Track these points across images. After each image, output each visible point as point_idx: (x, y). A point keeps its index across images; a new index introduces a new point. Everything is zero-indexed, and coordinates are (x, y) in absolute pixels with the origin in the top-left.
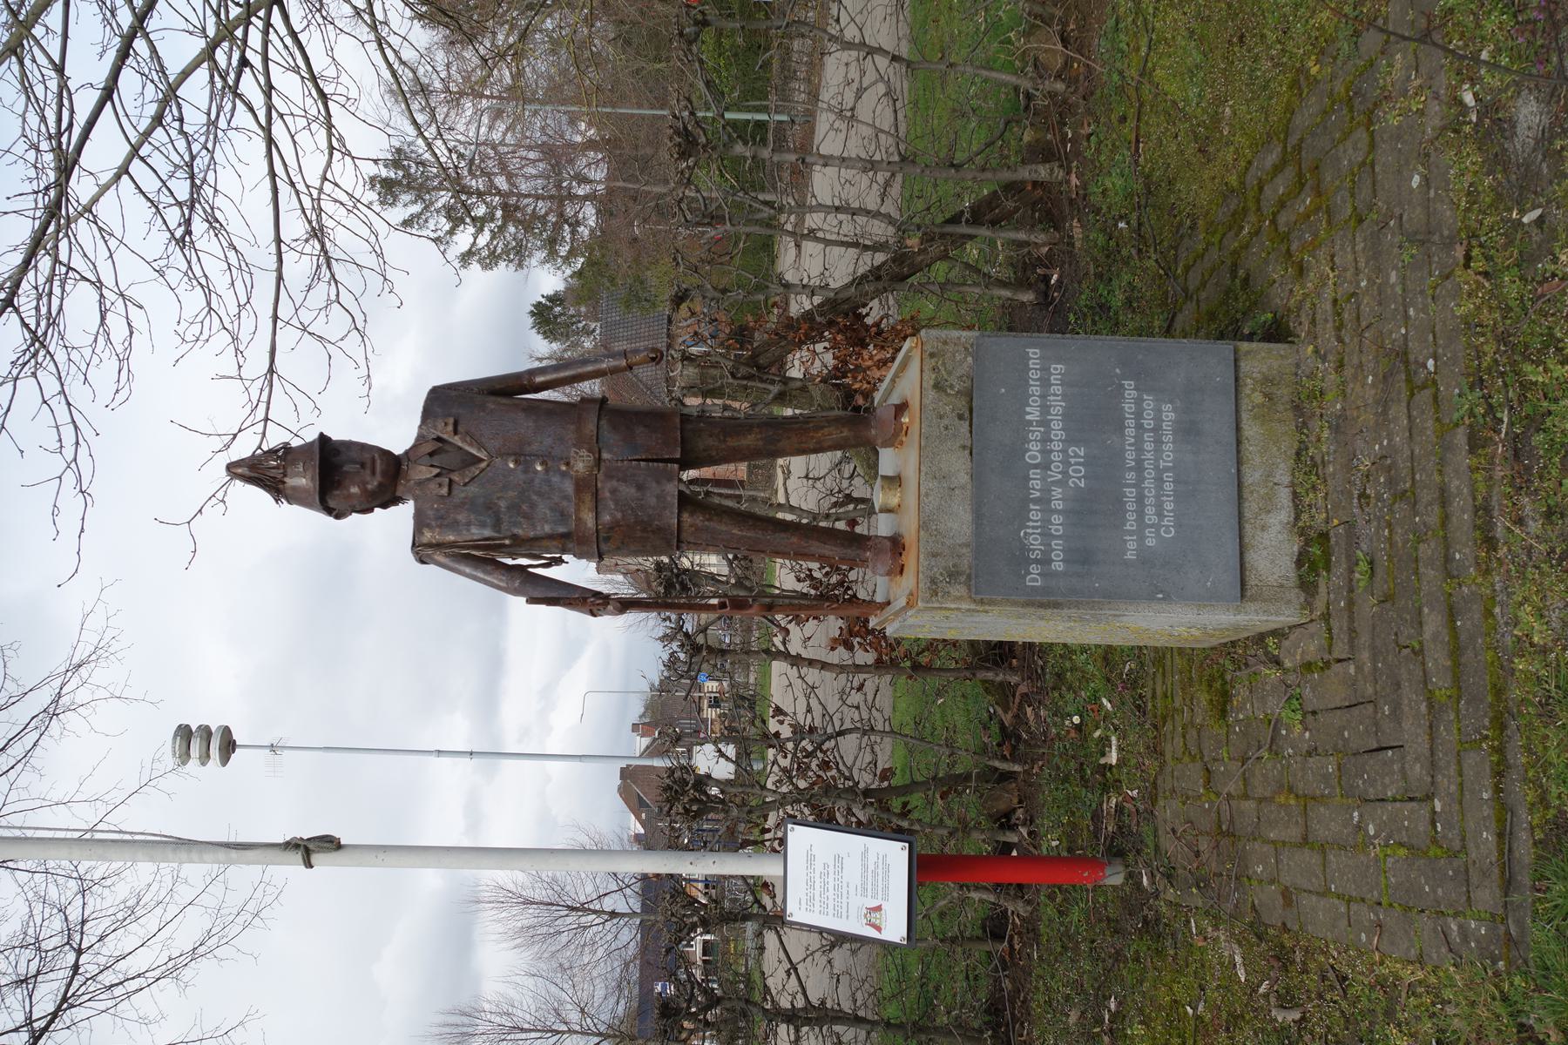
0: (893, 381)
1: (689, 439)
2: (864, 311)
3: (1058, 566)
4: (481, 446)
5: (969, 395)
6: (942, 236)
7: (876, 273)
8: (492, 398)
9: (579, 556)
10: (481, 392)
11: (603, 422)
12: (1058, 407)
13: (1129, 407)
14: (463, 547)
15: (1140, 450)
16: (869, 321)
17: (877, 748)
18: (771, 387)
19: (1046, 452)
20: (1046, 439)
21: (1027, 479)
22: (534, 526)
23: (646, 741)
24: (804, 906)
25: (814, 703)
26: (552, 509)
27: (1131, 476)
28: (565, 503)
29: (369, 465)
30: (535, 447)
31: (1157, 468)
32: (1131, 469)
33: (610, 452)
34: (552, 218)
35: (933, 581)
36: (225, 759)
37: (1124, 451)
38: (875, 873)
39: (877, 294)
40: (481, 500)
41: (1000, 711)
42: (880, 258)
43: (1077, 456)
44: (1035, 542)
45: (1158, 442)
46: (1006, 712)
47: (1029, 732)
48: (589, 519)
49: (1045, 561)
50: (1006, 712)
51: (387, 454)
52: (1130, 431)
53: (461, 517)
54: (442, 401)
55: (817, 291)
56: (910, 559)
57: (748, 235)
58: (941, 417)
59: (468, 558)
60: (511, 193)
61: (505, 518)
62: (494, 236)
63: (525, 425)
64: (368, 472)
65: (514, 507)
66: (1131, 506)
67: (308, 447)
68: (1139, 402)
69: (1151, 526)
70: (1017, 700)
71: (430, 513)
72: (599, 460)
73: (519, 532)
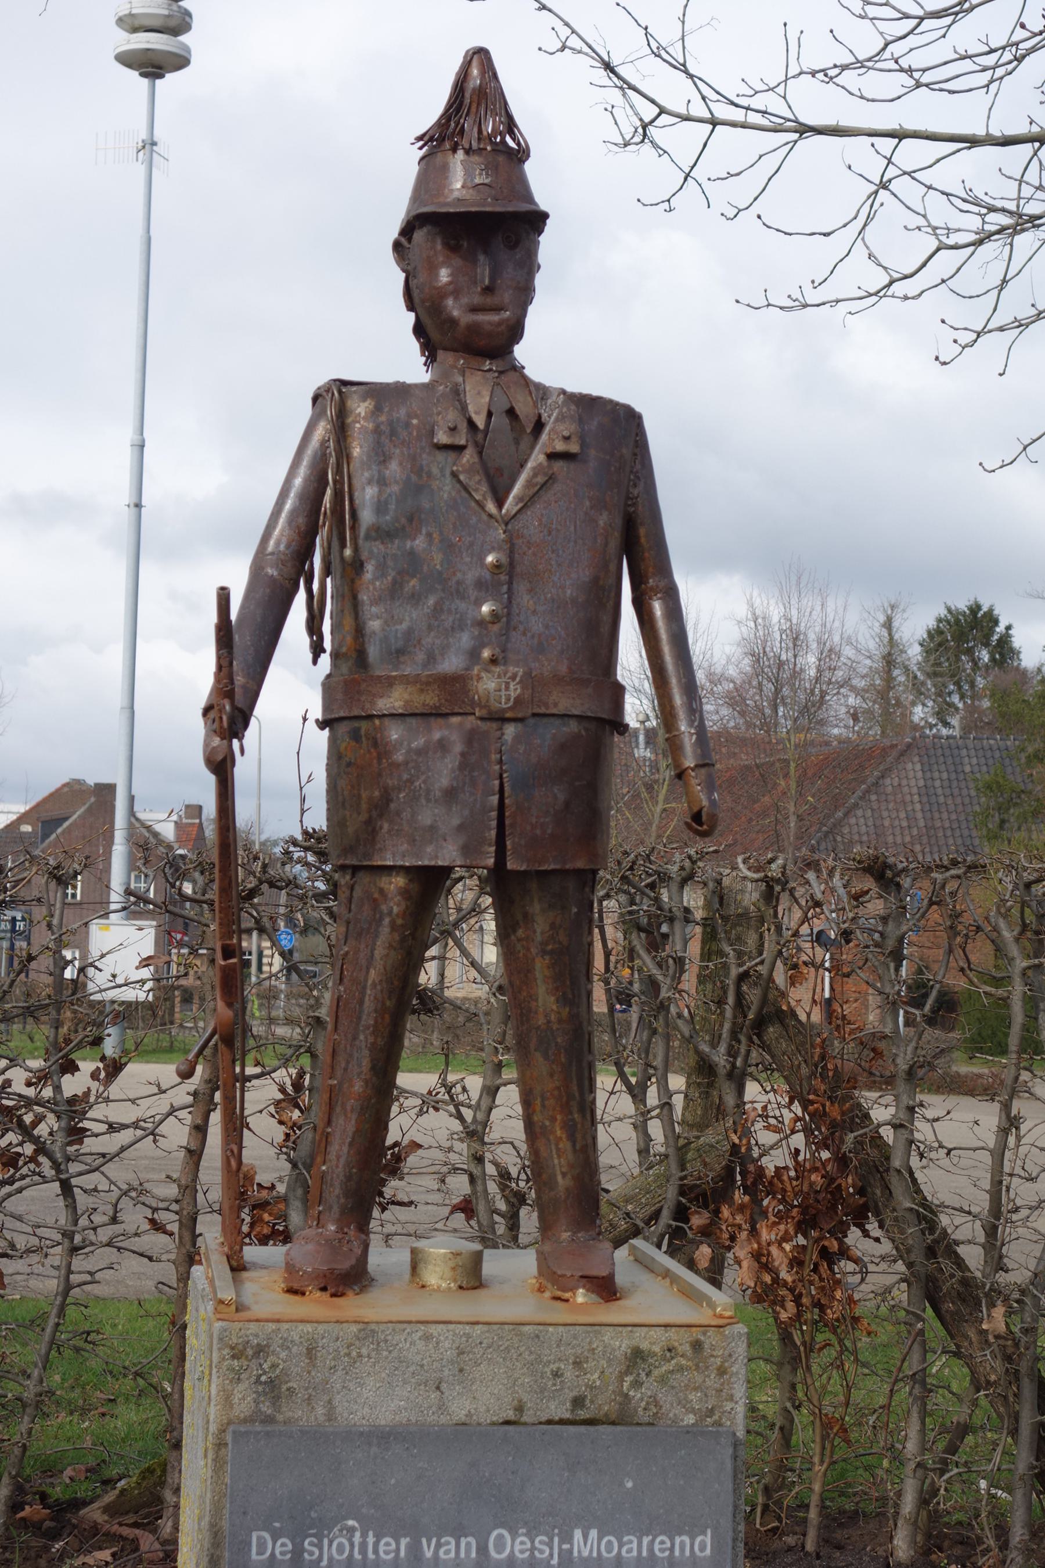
0: (667, 1274)
1: (545, 885)
2: (873, 1227)
4: (527, 503)
5: (621, 1418)
6: (1015, 1376)
7: (940, 1247)
8: (619, 522)
9: (328, 686)
10: (630, 500)
11: (573, 726)
14: (339, 470)
16: (854, 1235)
17: (35, 1258)
18: (722, 1048)
21: (458, 1533)
22: (375, 602)
23: (168, 831)
25: (126, 1136)
26: (409, 632)
28: (421, 657)
29: (489, 300)
30: (524, 599)
33: (517, 739)
35: (261, 1350)
36: (128, 60)
39: (902, 1252)
40: (426, 505)
41: (110, 1497)
42: (973, 1256)
46: (106, 1509)
47: (63, 1555)
48: (393, 701)
50: (106, 1509)
51: (515, 331)
53: (394, 468)
54: (613, 434)
55: (904, 1134)
56: (314, 1305)
57: (1005, 999)
58: (577, 1364)
59: (318, 482)
61: (394, 547)
63: (568, 580)
64: (477, 300)
65: (413, 563)
67: (522, 189)
70: (126, 1531)
71: (402, 412)
72: (500, 719)
73: (370, 568)
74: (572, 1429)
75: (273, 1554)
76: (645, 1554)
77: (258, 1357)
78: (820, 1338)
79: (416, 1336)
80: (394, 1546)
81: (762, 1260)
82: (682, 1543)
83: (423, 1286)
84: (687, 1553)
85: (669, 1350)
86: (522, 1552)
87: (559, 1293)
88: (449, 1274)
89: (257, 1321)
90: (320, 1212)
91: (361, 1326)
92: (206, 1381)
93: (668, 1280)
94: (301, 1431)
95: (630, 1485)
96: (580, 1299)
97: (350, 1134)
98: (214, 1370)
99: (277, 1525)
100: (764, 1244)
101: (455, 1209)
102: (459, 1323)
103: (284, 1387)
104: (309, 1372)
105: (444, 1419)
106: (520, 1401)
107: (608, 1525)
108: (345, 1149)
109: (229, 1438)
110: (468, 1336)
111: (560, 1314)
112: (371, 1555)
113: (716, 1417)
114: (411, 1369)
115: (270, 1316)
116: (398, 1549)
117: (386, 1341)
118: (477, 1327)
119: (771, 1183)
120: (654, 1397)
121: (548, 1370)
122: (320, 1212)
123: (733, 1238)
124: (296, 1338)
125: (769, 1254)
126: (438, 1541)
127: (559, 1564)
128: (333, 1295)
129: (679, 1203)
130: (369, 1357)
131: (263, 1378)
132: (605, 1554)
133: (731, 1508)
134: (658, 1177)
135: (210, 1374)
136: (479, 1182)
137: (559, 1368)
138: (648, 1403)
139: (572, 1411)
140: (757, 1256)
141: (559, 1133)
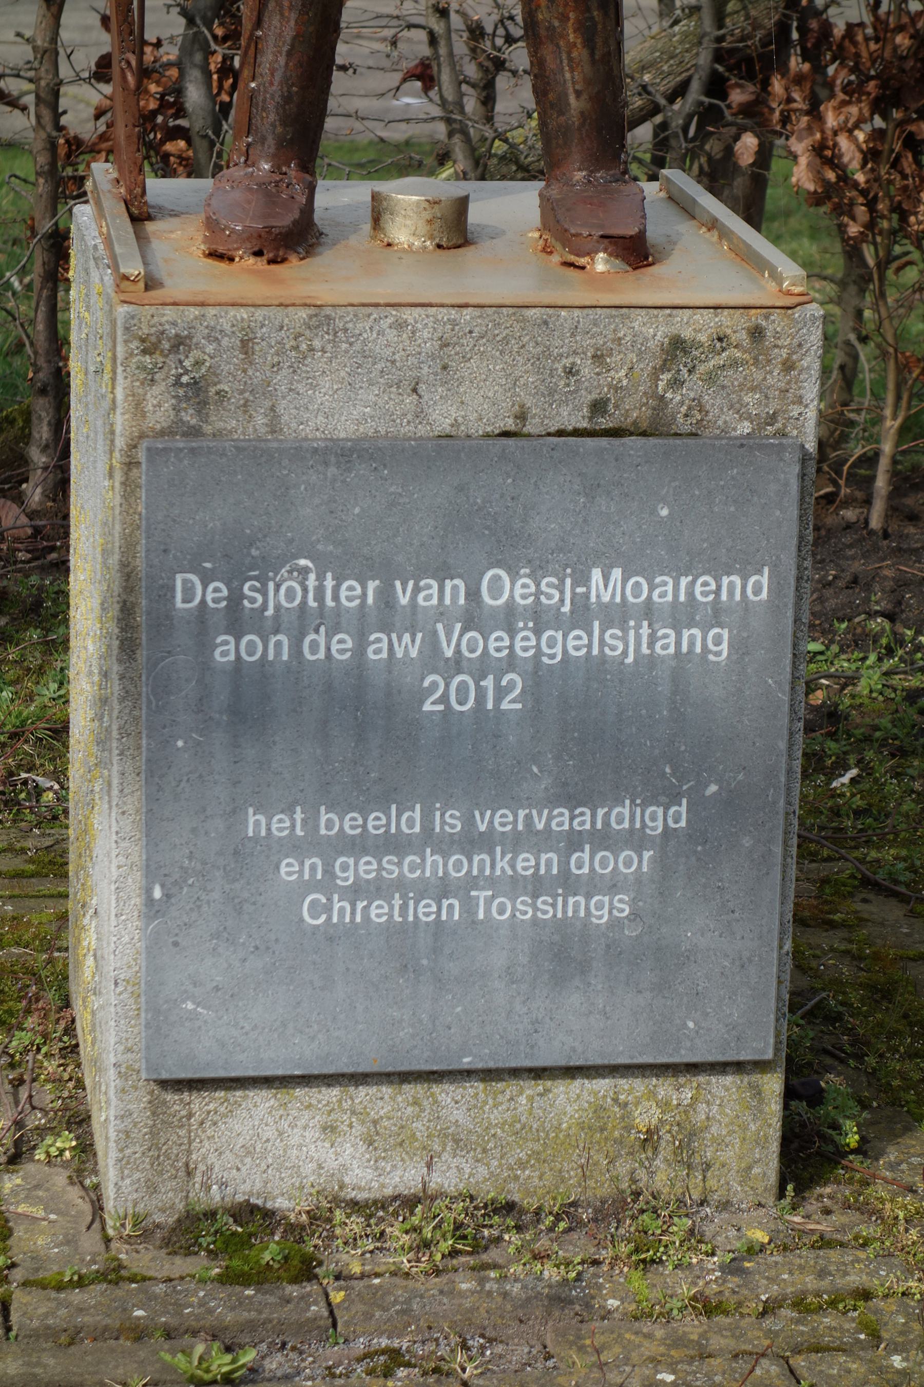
0: (713, 224)
12: (622, 645)
21: (442, 573)
35: (180, 343)
45: (536, 886)
49: (236, 619)
56: (246, 278)
58: (598, 358)
74: (589, 441)
75: (203, 602)
76: (682, 598)
77: (177, 352)
78: (898, 249)
79: (385, 324)
80: (359, 591)
81: (825, 154)
82: (731, 585)
83: (389, 245)
84: (738, 597)
85: (720, 339)
86: (524, 597)
87: (572, 258)
88: (423, 228)
89: (175, 304)
90: (249, 145)
91: (312, 311)
92: (107, 376)
93: (715, 233)
94: (237, 448)
95: (664, 512)
96: (600, 267)
97: (288, 39)
98: (120, 369)
99: (208, 565)
100: (829, 133)
101: (410, 76)
102: (442, 306)
103: (213, 390)
104: (245, 371)
105: (422, 430)
106: (522, 406)
108: (282, 60)
109: (142, 456)
110: (454, 323)
111: (575, 291)
112: (330, 603)
113: (779, 425)
114: (378, 367)
115: (190, 298)
116: (364, 595)
117: (346, 330)
118: (465, 311)
119: (841, 46)
120: (698, 400)
121: (559, 366)
122: (249, 145)
123: (785, 120)
124: (227, 327)
125: (835, 145)
126: (416, 586)
127: (572, 612)
128: (271, 262)
129: (714, 74)
130: (323, 351)
131: (185, 379)
132: (631, 599)
133: (795, 541)
134: (686, 35)
135: (114, 372)
136: (442, 43)
137: (573, 364)
138: (689, 408)
139: (591, 419)
140: (818, 150)
141: (571, 37)
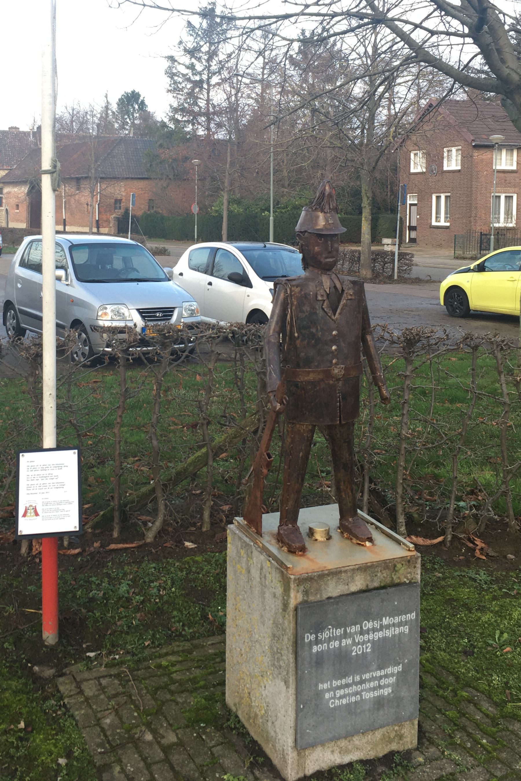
3: (315, 649)
12: (388, 633)
13: (389, 670)
15: (370, 680)
19: (368, 632)
20: (374, 630)
24: (30, 464)
27: (358, 678)
31: (362, 691)
32: (361, 678)
34: (196, 109)
37: (369, 672)
38: (57, 510)
43: (367, 648)
44: (326, 635)
45: (374, 689)
49: (317, 642)
52: (378, 673)
60: (209, 85)
62: (184, 75)
66: (344, 681)
68: (392, 675)
69: (335, 695)
107: (391, 615)
